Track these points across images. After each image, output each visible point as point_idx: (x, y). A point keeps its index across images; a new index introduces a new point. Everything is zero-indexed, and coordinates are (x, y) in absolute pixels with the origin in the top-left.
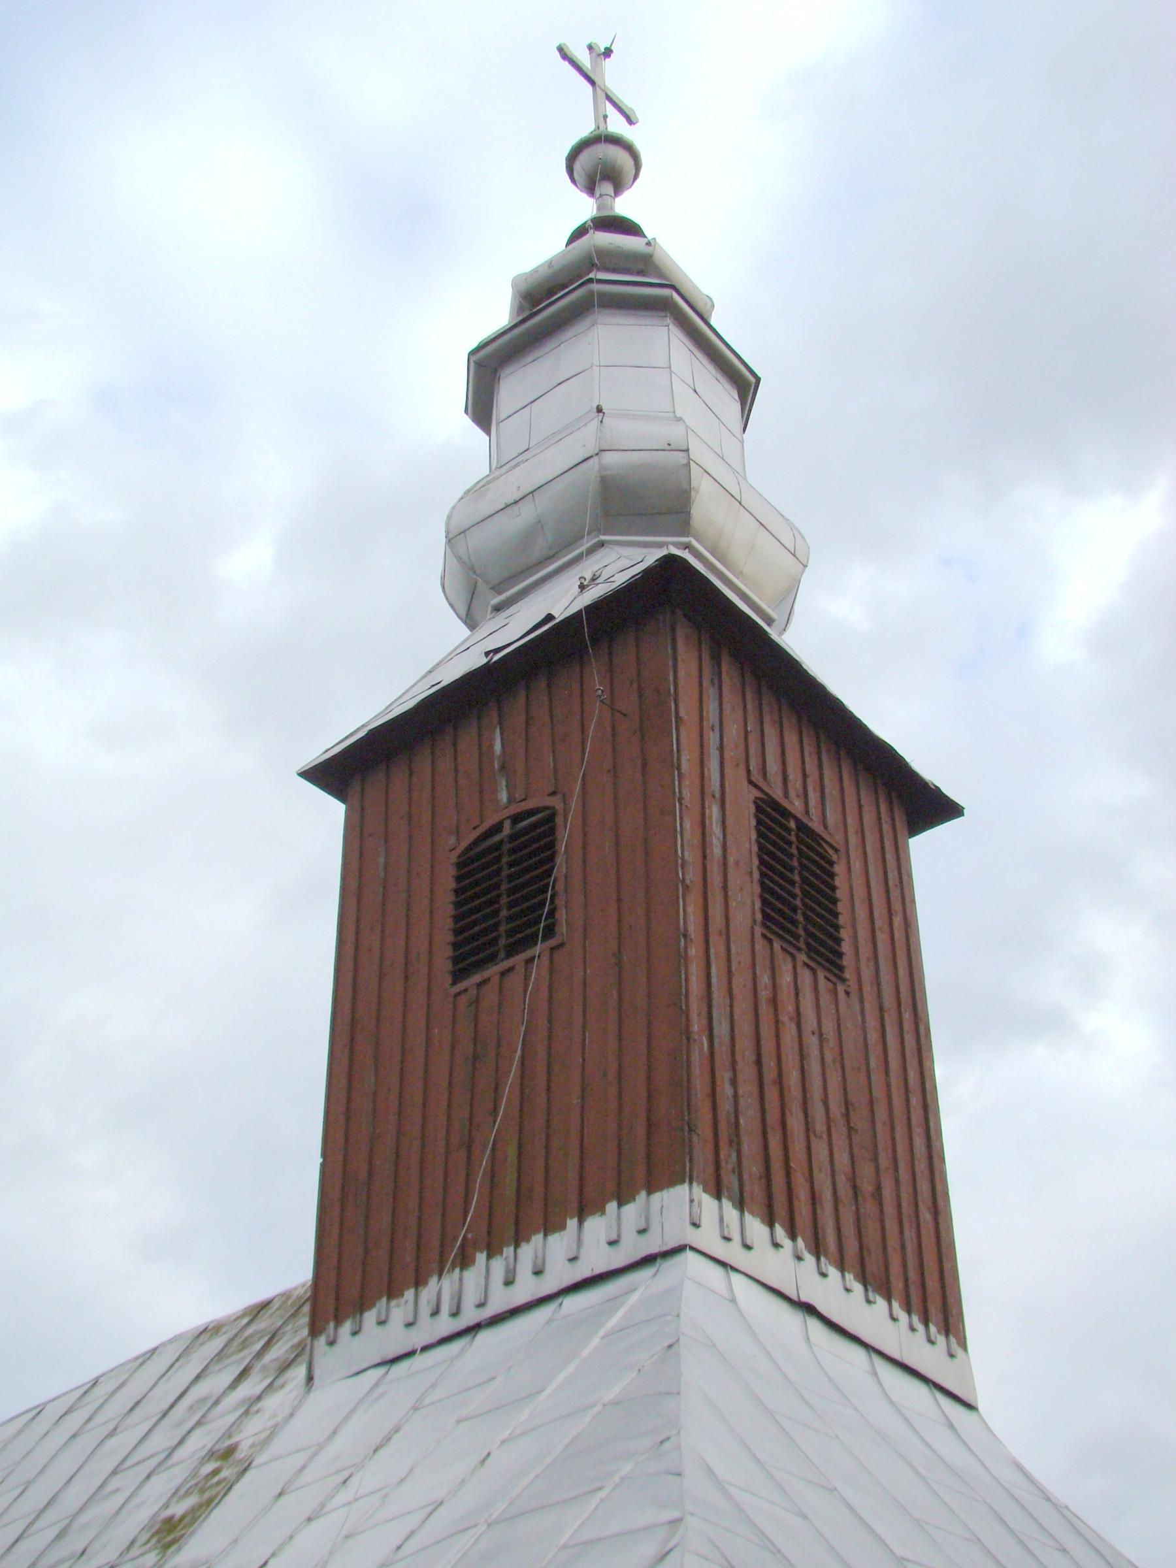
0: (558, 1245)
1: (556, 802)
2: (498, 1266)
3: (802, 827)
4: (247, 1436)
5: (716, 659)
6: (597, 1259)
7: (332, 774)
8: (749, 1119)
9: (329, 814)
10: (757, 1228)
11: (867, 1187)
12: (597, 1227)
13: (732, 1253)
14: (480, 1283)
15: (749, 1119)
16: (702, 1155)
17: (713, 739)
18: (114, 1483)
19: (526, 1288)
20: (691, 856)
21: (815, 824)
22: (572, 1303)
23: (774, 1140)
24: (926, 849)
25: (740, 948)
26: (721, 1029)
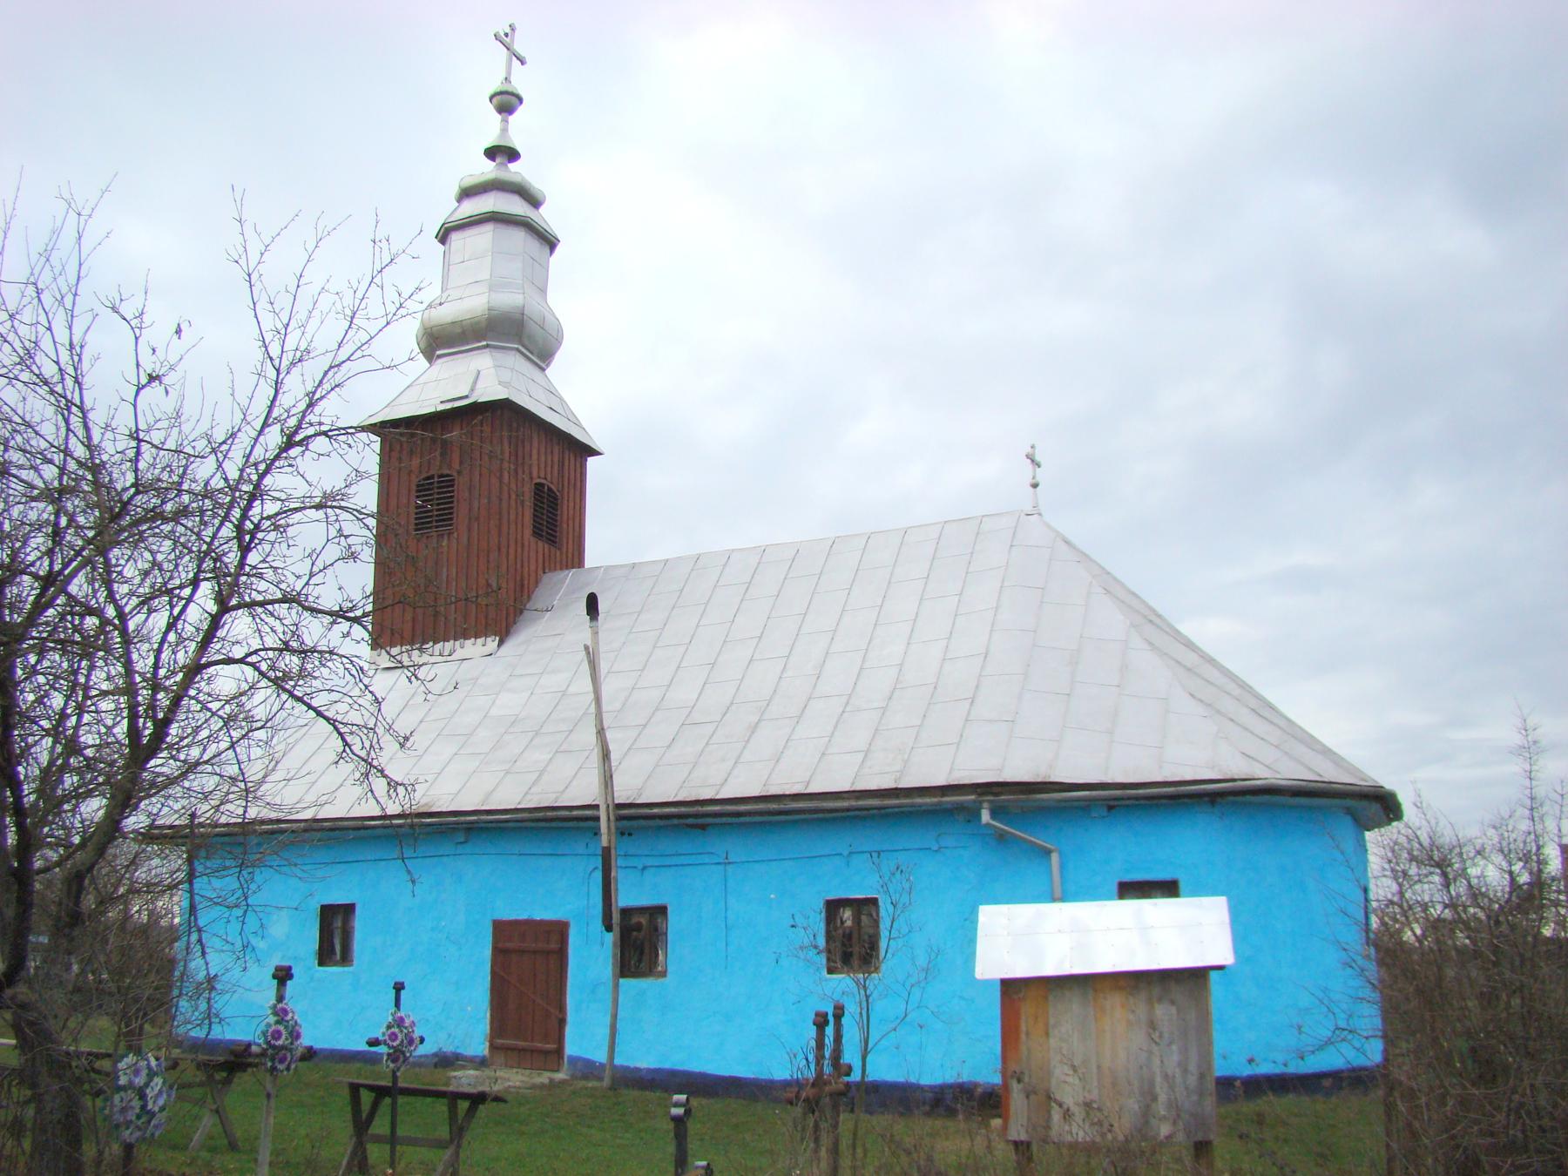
24: (591, 461)
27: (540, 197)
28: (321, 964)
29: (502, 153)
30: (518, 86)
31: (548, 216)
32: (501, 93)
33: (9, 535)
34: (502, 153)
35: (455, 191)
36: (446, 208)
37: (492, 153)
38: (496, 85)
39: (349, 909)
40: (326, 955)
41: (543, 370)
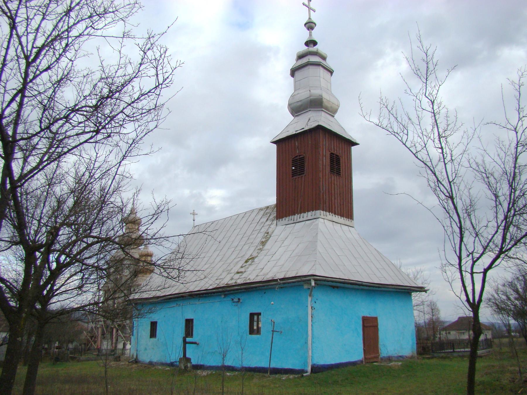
0: (305, 215)
1: (304, 155)
2: (298, 216)
3: (336, 155)
4: (270, 231)
5: (325, 134)
6: (309, 218)
7: (274, 142)
8: (327, 200)
9: (275, 146)
10: (328, 213)
11: (342, 203)
12: (310, 213)
13: (325, 217)
14: (296, 217)
15: (327, 200)
16: (321, 206)
17: (324, 147)
18: (253, 233)
19: (301, 219)
20: (321, 167)
21: (338, 154)
22: (307, 222)
23: (330, 203)
24: (353, 148)
25: (327, 177)
26: (324, 189)
27: (325, 55)
28: (250, 334)
29: (311, 43)
30: (314, 19)
31: (329, 63)
32: (309, 22)
33: (20, 309)
34: (311, 43)
35: (295, 57)
36: (292, 62)
37: (307, 44)
38: (306, 20)
39: (259, 314)
40: (252, 331)
41: (333, 116)
